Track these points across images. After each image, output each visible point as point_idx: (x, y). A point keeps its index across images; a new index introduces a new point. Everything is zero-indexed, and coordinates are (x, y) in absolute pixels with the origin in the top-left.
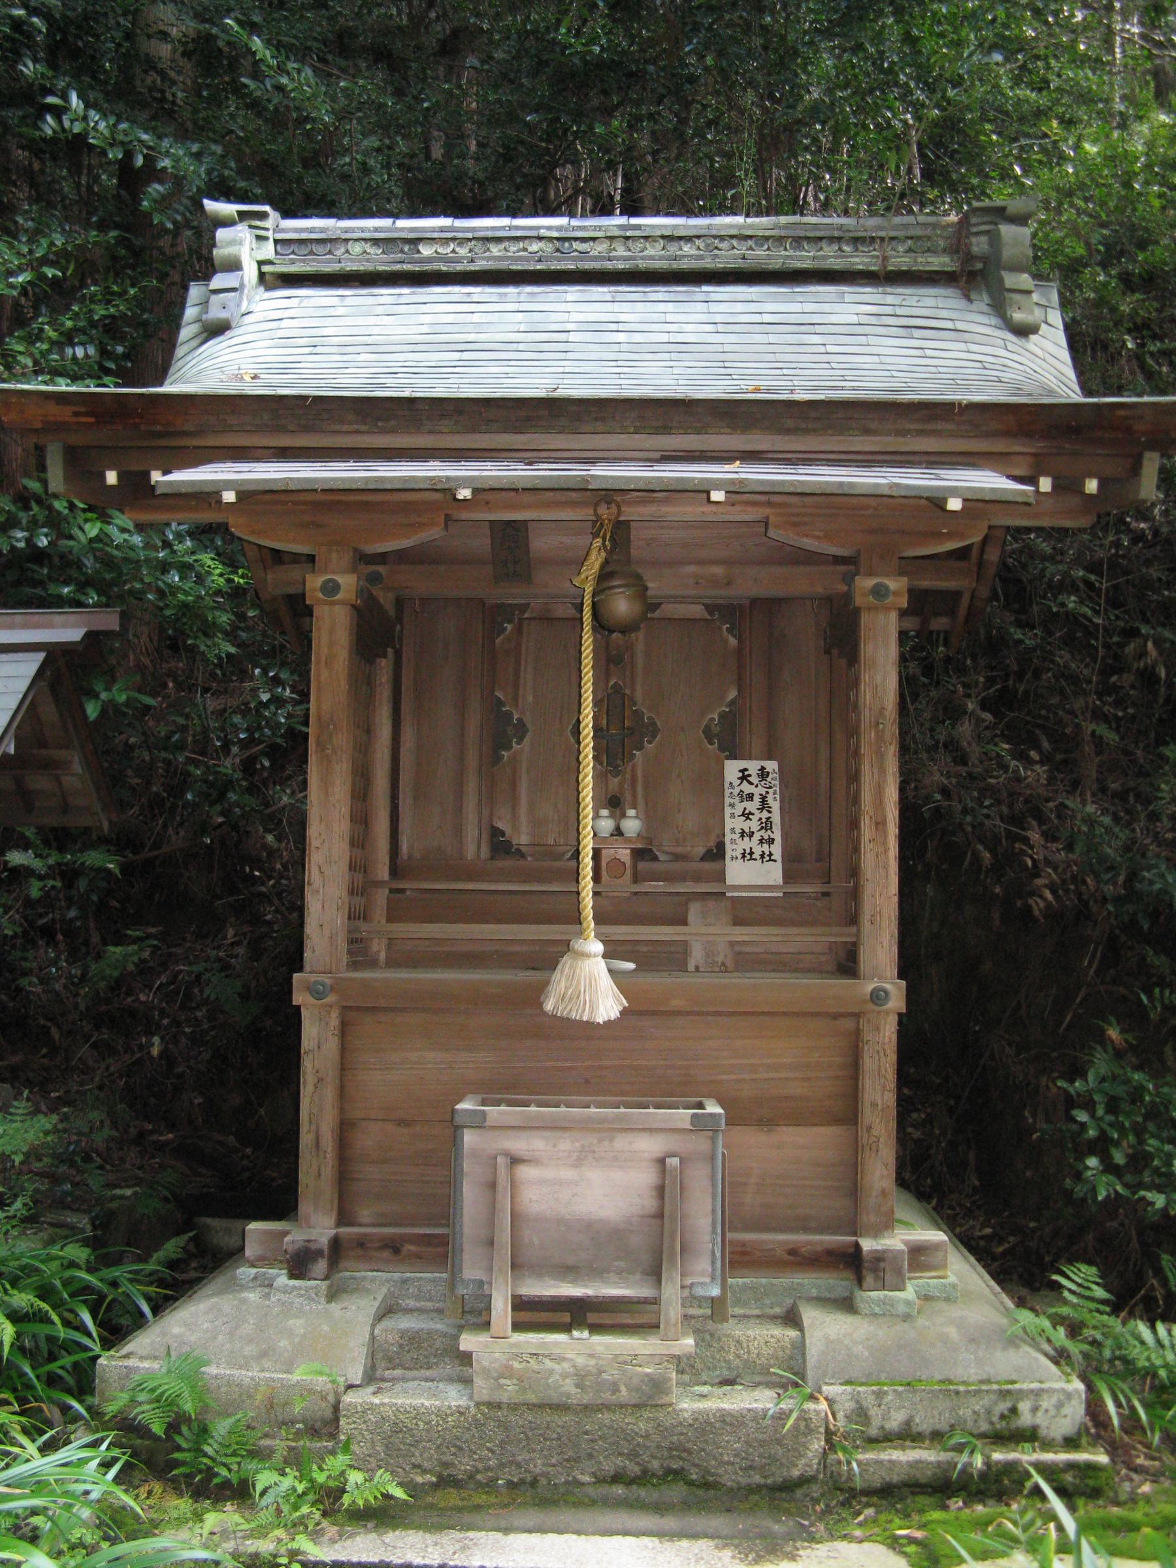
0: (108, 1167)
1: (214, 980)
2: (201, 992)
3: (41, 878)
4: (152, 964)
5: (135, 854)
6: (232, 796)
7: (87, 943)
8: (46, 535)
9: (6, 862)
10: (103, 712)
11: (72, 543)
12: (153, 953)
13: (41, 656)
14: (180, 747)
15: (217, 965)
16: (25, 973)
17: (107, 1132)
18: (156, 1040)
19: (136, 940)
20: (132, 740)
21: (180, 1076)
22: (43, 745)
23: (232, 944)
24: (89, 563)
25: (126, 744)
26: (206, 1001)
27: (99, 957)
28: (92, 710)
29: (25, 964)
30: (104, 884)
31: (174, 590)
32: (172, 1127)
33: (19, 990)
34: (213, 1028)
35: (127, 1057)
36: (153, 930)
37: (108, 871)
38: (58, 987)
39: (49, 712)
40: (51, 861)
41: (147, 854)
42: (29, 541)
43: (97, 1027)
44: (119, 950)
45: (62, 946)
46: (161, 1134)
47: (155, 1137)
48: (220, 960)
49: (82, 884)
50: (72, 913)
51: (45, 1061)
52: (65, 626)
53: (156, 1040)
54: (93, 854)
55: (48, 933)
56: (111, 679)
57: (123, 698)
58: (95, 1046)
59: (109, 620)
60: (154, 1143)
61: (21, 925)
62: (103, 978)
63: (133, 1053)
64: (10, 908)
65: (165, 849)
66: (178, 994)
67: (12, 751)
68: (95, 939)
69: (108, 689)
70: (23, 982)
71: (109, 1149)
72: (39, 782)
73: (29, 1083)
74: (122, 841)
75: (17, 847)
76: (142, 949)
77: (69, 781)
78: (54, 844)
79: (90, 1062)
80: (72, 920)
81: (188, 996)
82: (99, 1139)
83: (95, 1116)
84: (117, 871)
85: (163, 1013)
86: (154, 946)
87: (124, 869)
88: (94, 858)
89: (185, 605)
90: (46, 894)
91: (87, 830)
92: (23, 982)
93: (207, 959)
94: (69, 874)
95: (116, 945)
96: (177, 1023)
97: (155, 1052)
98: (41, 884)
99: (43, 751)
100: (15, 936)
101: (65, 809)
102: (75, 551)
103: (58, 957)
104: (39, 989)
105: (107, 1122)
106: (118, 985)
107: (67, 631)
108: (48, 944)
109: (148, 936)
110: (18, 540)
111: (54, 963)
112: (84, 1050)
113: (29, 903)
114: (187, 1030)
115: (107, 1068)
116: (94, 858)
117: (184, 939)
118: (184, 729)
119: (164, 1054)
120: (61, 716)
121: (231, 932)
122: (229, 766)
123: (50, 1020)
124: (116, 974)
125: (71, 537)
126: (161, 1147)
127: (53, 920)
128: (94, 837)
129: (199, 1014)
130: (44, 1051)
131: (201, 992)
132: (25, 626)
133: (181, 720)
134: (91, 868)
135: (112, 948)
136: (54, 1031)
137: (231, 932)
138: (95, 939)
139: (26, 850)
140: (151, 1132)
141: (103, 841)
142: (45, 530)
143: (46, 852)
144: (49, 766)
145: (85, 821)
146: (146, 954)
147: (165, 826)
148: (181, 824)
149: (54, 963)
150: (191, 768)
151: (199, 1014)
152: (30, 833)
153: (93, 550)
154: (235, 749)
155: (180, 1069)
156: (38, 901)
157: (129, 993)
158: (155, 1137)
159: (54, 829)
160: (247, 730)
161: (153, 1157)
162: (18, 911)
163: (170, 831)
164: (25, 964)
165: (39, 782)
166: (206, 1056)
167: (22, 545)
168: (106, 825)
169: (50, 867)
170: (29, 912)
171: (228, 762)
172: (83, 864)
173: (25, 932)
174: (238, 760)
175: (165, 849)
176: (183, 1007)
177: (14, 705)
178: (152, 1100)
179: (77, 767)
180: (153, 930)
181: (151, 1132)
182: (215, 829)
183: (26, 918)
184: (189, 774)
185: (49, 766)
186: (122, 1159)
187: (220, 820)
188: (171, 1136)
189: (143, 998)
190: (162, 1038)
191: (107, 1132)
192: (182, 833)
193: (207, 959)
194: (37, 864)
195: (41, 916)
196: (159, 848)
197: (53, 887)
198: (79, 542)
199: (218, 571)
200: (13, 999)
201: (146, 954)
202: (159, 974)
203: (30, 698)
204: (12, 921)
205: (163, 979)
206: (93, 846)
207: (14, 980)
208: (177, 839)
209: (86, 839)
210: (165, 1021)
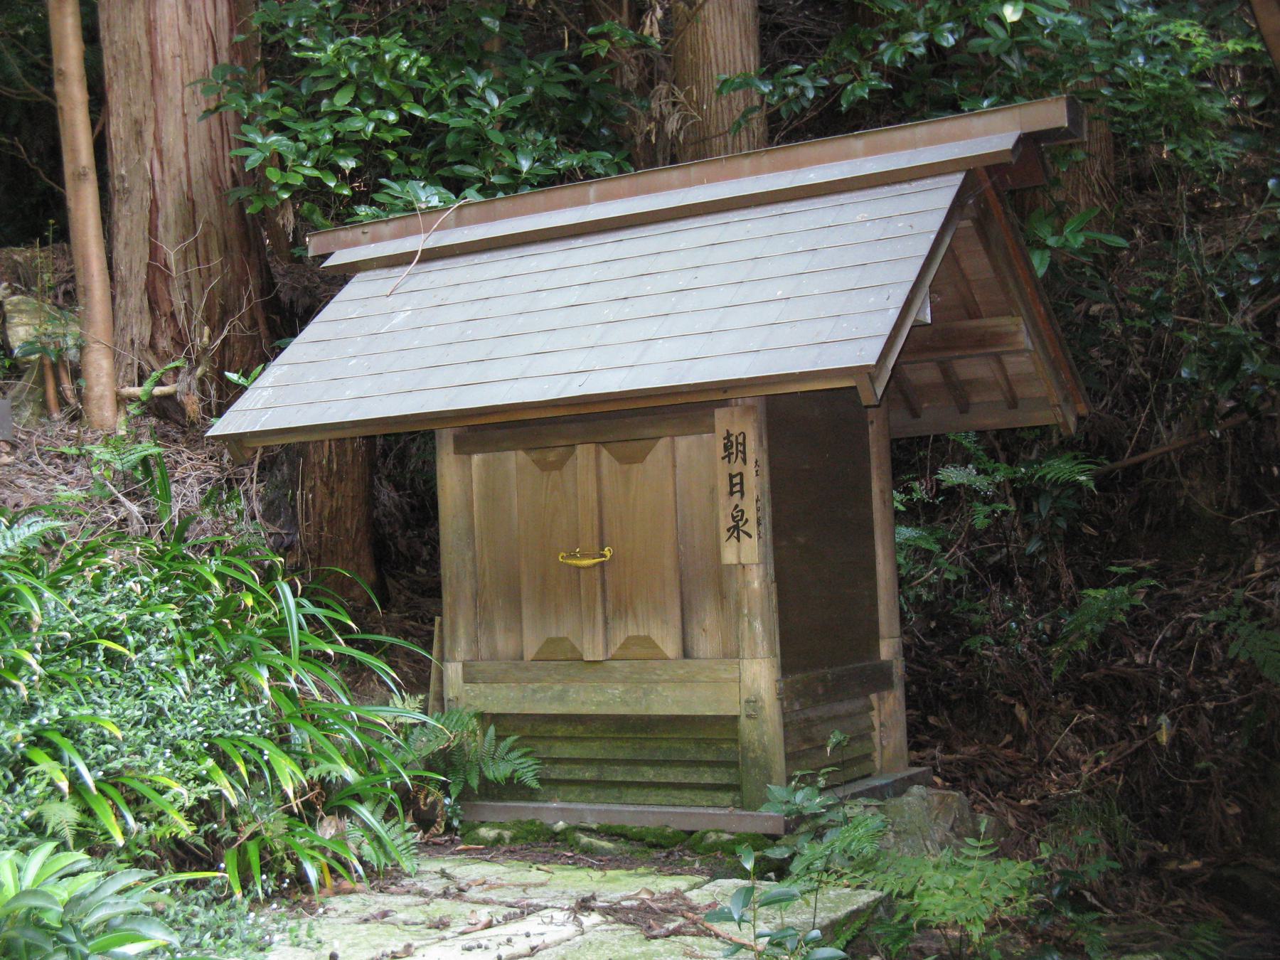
0: (1110, 913)
1: (1242, 632)
2: (1225, 649)
3: (987, 501)
4: (1148, 610)
5: (1112, 461)
6: (1248, 367)
7: (1055, 586)
8: (952, 32)
9: (939, 482)
10: (1052, 267)
11: (987, 41)
12: (1148, 596)
13: (958, 178)
14: (1163, 307)
15: (1246, 612)
16: (975, 632)
17: (1104, 863)
18: (1164, 720)
19: (1123, 580)
20: (1095, 309)
21: (1205, 773)
22: (974, 314)
23: (1262, 579)
24: (1013, 62)
25: (1086, 315)
26: (1232, 663)
27: (1074, 604)
28: (1040, 264)
29: (976, 618)
30: (1072, 504)
31: (1139, 76)
32: (1197, 848)
33: (969, 653)
34: (1247, 702)
35: (1124, 744)
36: (1146, 564)
37: (1078, 486)
38: (1022, 648)
39: (977, 264)
40: (999, 478)
41: (1127, 460)
42: (931, 44)
43: (1079, 703)
44: (1101, 593)
45: (1023, 592)
46: (1182, 861)
47: (1172, 865)
48: (1247, 602)
49: (1043, 507)
50: (1033, 547)
51: (1009, 752)
52: (987, 133)
53: (1164, 720)
54: (1056, 463)
55: (1003, 575)
56: (1060, 215)
57: (1078, 241)
58: (1077, 730)
59: (1050, 113)
60: (1173, 873)
61: (966, 567)
62: (1083, 636)
63: (1132, 740)
64: (950, 543)
65: (1154, 451)
66: (1189, 651)
67: (928, 320)
68: (1067, 579)
69: (1058, 232)
70: (974, 643)
71: (1107, 883)
72: (973, 368)
73: (991, 786)
74: (1092, 443)
75: (953, 461)
76: (1132, 593)
77: (1018, 365)
78: (1002, 456)
79: (1071, 753)
80: (1032, 556)
81: (1205, 656)
82: (1094, 870)
83: (1084, 837)
84: (1092, 485)
85: (1169, 679)
86: (1150, 587)
87: (1103, 482)
88: (1060, 468)
89: (1158, 97)
90: (997, 522)
91: (1045, 431)
92: (974, 643)
93: (1230, 602)
94: (1025, 494)
95: (1096, 587)
96: (1191, 695)
97: (1164, 738)
98: (988, 509)
99: (974, 323)
100: (960, 580)
101: (1013, 403)
102: (992, 50)
103: (1018, 607)
104: (994, 652)
105: (1104, 845)
106: (1106, 643)
107: (990, 133)
108: (1004, 591)
109: (1140, 573)
110: (916, 46)
111: (1014, 614)
112: (1064, 738)
113: (973, 535)
114: (1209, 706)
115: (1097, 762)
116: (1060, 468)
117: (1191, 574)
118: (1165, 285)
119: (1177, 740)
120: (996, 269)
121: (1260, 562)
122: (1238, 324)
123: (1012, 695)
124: (1099, 628)
125: (986, 34)
126: (1183, 880)
127: (1009, 556)
128: (1055, 441)
129: (1224, 681)
130: (1008, 738)
131: (1225, 649)
132: (932, 141)
133: (1158, 276)
134: (1055, 484)
135: (1091, 592)
136: (1021, 713)
137: (1260, 562)
138: (1067, 579)
139: (965, 464)
140: (1168, 857)
141: (1067, 446)
142: (949, 25)
143: (990, 466)
144: (985, 342)
145: (1042, 417)
146: (1139, 600)
147: (1151, 419)
148: (1174, 416)
149: (1014, 614)
150: (1184, 334)
151: (1224, 681)
152: (968, 443)
153: (1021, 47)
154: (1244, 303)
155: (1202, 765)
156: (987, 531)
157: (1120, 652)
158: (1172, 865)
159: (999, 433)
160: (1260, 273)
161: (1173, 896)
162: (960, 546)
163: (1160, 425)
164: (976, 618)
165: (973, 368)
166: (1241, 743)
167: (921, 50)
168: (1072, 420)
169: (998, 486)
170: (975, 546)
171: (1237, 321)
172: (1042, 478)
173: (973, 577)
174: (1249, 319)
175: (1154, 451)
176: (1199, 672)
177: (924, 249)
178: (1165, 809)
179: (1024, 340)
180: (1146, 564)
181: (1168, 857)
182: (1224, 417)
183: (971, 555)
184: (1181, 343)
185: (985, 342)
186: (1129, 900)
187: (1230, 404)
188: (1196, 864)
189: (1139, 659)
190: (1173, 718)
191: (1104, 863)
192: (1175, 427)
193: (1230, 602)
194: (981, 483)
195: (991, 552)
196: (1144, 450)
197: (1005, 513)
198: (996, 38)
199: (1201, 40)
200: (962, 666)
201: (1139, 600)
202: (1160, 625)
203: (947, 240)
204: (954, 562)
205: (1167, 631)
206: (1052, 453)
207: (962, 640)
208: (1170, 439)
209: (1042, 440)
210: (1175, 693)
